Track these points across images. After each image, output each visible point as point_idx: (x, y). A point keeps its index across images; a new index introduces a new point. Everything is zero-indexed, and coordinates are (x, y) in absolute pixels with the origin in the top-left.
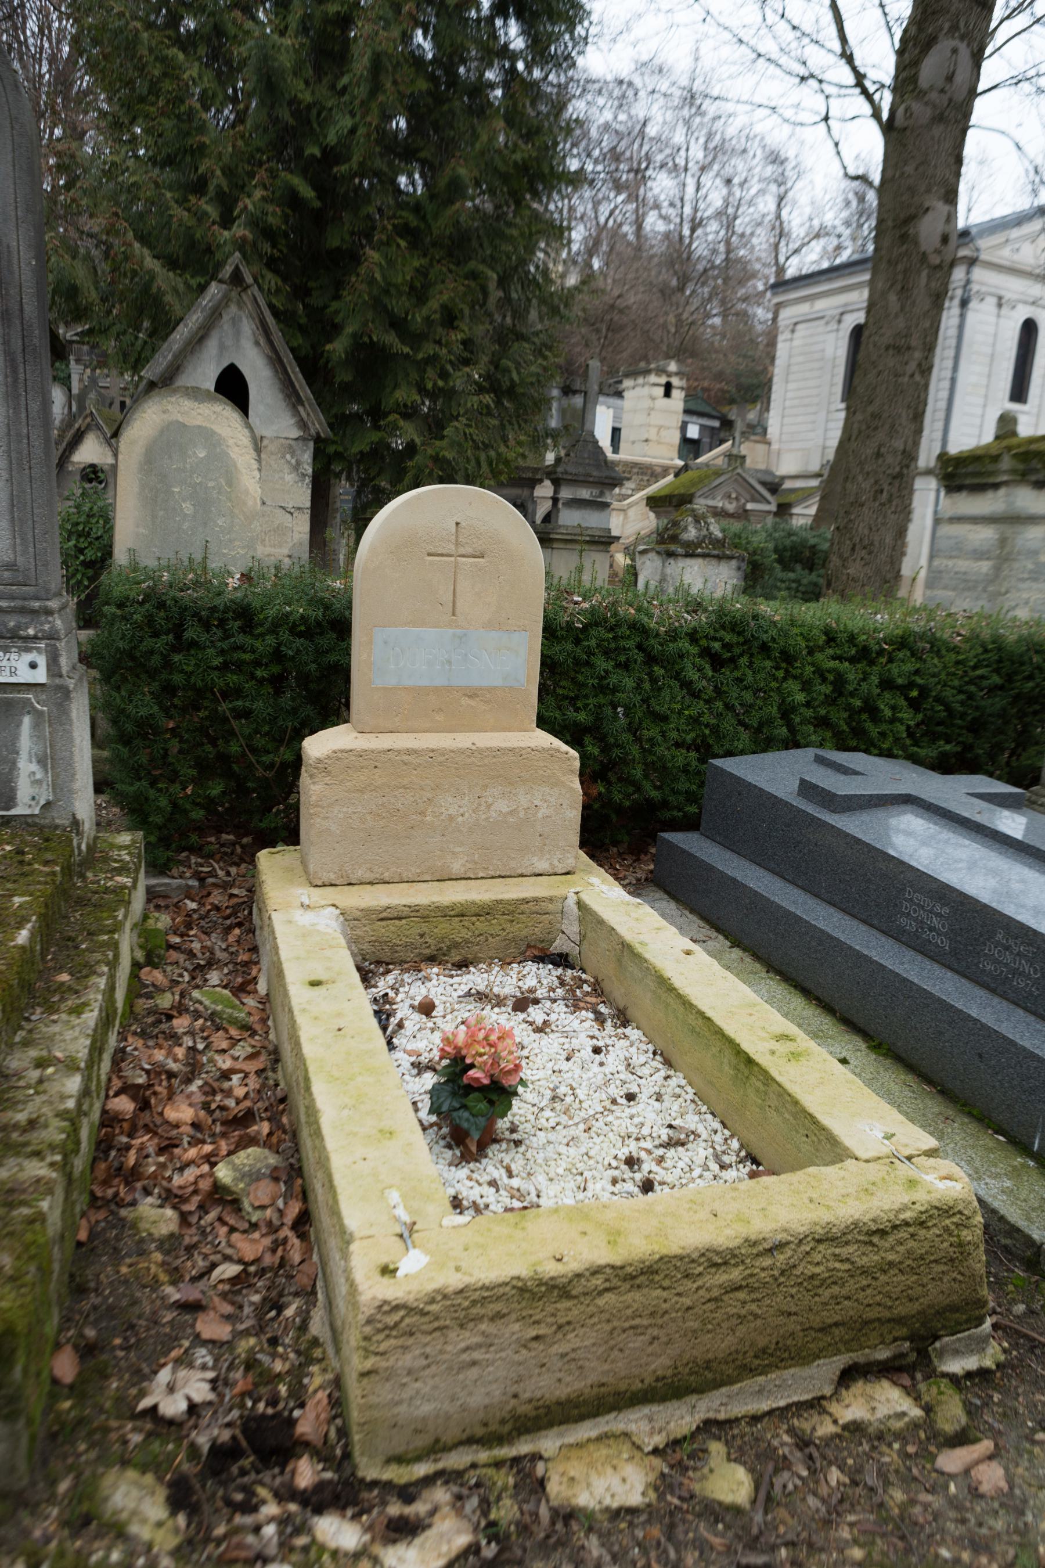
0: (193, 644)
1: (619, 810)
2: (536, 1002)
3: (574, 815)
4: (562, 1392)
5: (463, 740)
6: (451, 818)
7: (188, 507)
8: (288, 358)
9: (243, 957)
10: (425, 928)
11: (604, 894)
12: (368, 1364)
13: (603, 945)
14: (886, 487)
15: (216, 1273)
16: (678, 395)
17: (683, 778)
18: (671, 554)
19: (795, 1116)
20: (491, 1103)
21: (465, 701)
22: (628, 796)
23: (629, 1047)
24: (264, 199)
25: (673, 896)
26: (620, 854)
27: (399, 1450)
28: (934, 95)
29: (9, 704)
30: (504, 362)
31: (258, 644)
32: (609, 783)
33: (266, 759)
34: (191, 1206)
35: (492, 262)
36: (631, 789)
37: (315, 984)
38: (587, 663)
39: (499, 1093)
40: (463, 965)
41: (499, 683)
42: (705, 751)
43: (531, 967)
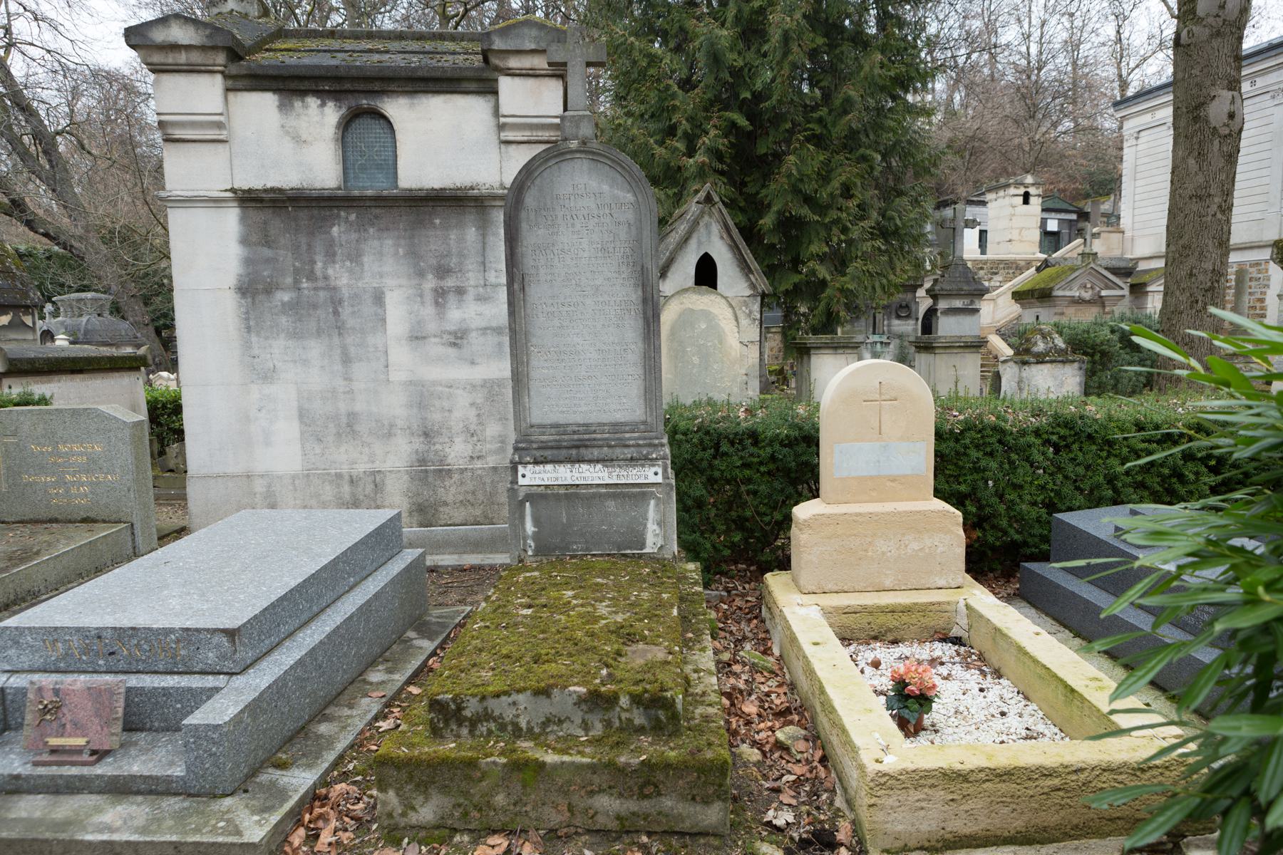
0: (726, 454)
1: (993, 548)
2: (942, 664)
3: (961, 551)
4: (967, 831)
5: (888, 507)
6: (883, 553)
7: (696, 360)
8: (735, 232)
9: (761, 635)
10: (870, 619)
11: (983, 599)
12: (873, 801)
13: (983, 630)
14: (1200, 298)
15: (784, 779)
16: (1036, 202)
17: (1037, 526)
18: (1025, 363)
19: (1098, 718)
20: (921, 705)
21: (889, 484)
22: (997, 539)
23: (1001, 690)
24: (716, 136)
25: (1033, 604)
26: (996, 578)
27: (888, 847)
28: (1210, 20)
29: (644, 494)
30: (889, 213)
31: (761, 452)
32: (984, 530)
33: (767, 519)
34: (767, 748)
35: (875, 146)
36: (1000, 534)
37: (816, 644)
38: (965, 454)
39: (924, 700)
40: (895, 642)
41: (909, 472)
42: (1052, 507)
43: (937, 645)
